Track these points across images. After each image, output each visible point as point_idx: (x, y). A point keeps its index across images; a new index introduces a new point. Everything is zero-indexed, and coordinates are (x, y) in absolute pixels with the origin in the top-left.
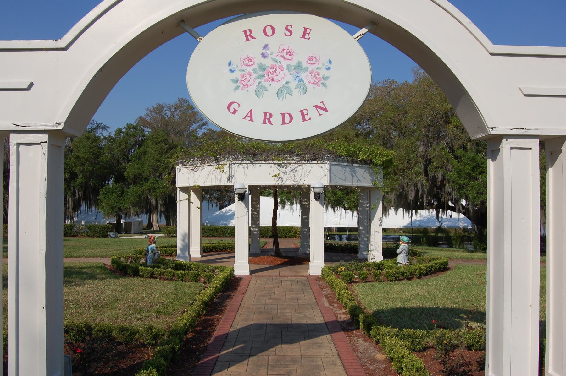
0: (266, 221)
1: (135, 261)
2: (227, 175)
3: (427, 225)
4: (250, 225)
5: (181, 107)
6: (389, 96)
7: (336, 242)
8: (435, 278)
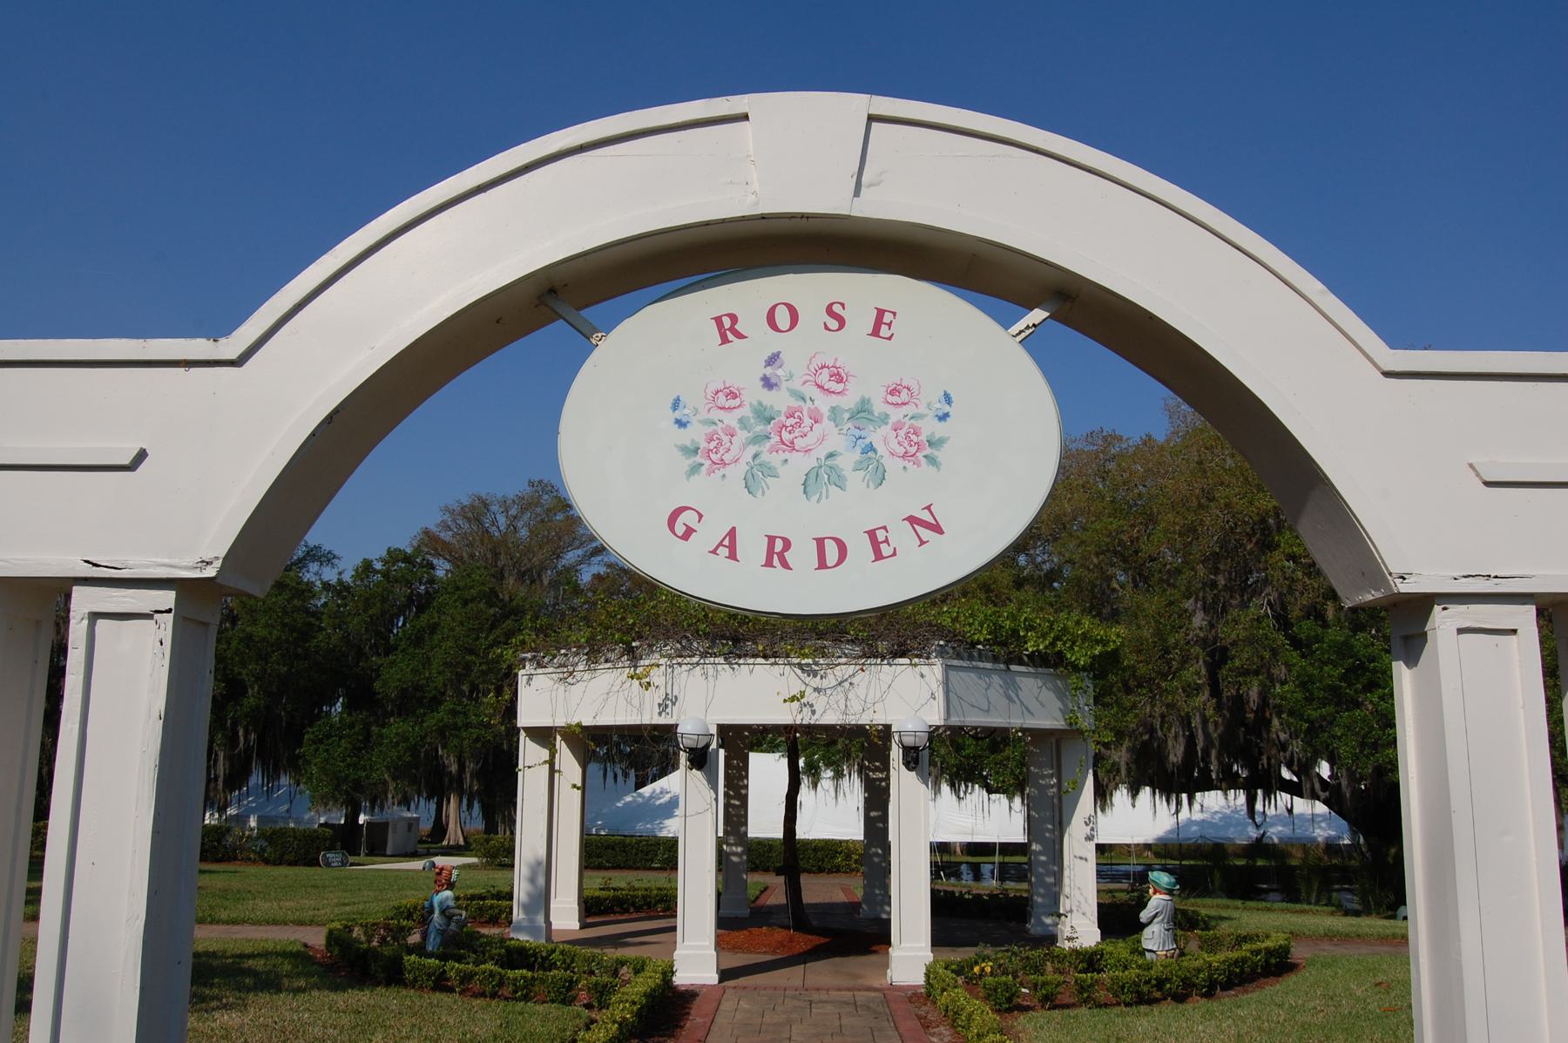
0: (765, 823)
1: (394, 939)
2: (658, 697)
3: (1222, 834)
4: (721, 834)
5: (538, 504)
6: (1104, 475)
7: (964, 885)
8: (1255, 995)
